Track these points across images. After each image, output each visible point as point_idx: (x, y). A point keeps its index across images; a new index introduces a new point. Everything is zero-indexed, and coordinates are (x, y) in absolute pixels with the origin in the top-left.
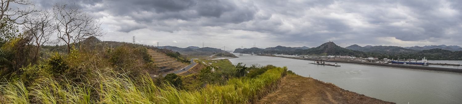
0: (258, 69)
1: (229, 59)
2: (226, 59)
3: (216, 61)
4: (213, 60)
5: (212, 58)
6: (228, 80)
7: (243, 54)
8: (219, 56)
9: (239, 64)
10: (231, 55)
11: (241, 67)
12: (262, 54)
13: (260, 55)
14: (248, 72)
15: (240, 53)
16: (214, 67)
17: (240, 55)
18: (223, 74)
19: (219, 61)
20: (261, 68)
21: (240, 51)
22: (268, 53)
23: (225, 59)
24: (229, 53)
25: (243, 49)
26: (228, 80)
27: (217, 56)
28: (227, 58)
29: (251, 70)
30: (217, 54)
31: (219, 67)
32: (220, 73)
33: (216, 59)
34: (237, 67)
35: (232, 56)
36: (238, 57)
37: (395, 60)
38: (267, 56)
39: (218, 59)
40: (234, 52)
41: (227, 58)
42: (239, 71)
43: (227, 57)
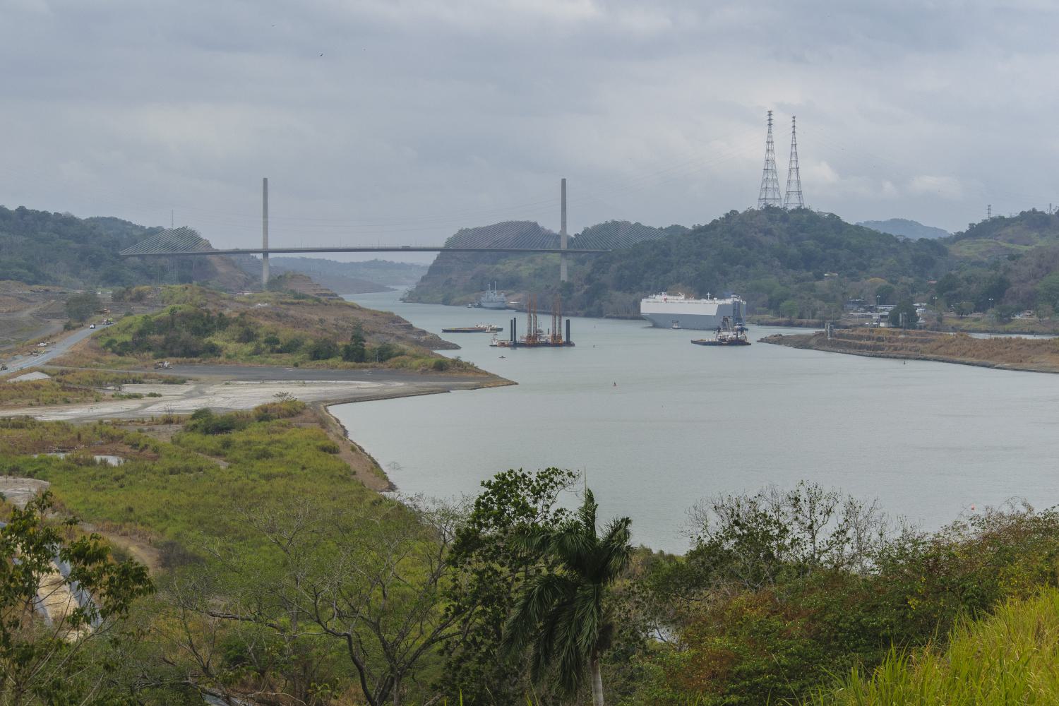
0: (836, 578)
1: (335, 411)
2: (291, 412)
3: (109, 435)
4: (70, 436)
5: (32, 394)
6: (365, 341)
7: (581, 328)
8: (166, 350)
9: (504, 487)
10: (371, 344)
11: (542, 540)
12: (904, 319)
13: (874, 347)
14: (662, 635)
15: (533, 308)
16: (81, 554)
17: (533, 342)
18: (237, 659)
19: (164, 437)
20: (886, 560)
21: (525, 269)
22: (1005, 318)
23: (264, 414)
24: (327, 301)
25: (573, 230)
26: (365, 341)
27: (123, 350)
28: (301, 392)
29: (707, 601)
30: (137, 318)
31: (172, 556)
32: (179, 657)
33: (107, 409)
34: (468, 542)
35: (384, 354)
36: (482, 379)
37: (1043, 340)
38: (987, 357)
39: (157, 409)
40: (414, 297)
41: (301, 392)
42: (496, 621)
43: (302, 378)
